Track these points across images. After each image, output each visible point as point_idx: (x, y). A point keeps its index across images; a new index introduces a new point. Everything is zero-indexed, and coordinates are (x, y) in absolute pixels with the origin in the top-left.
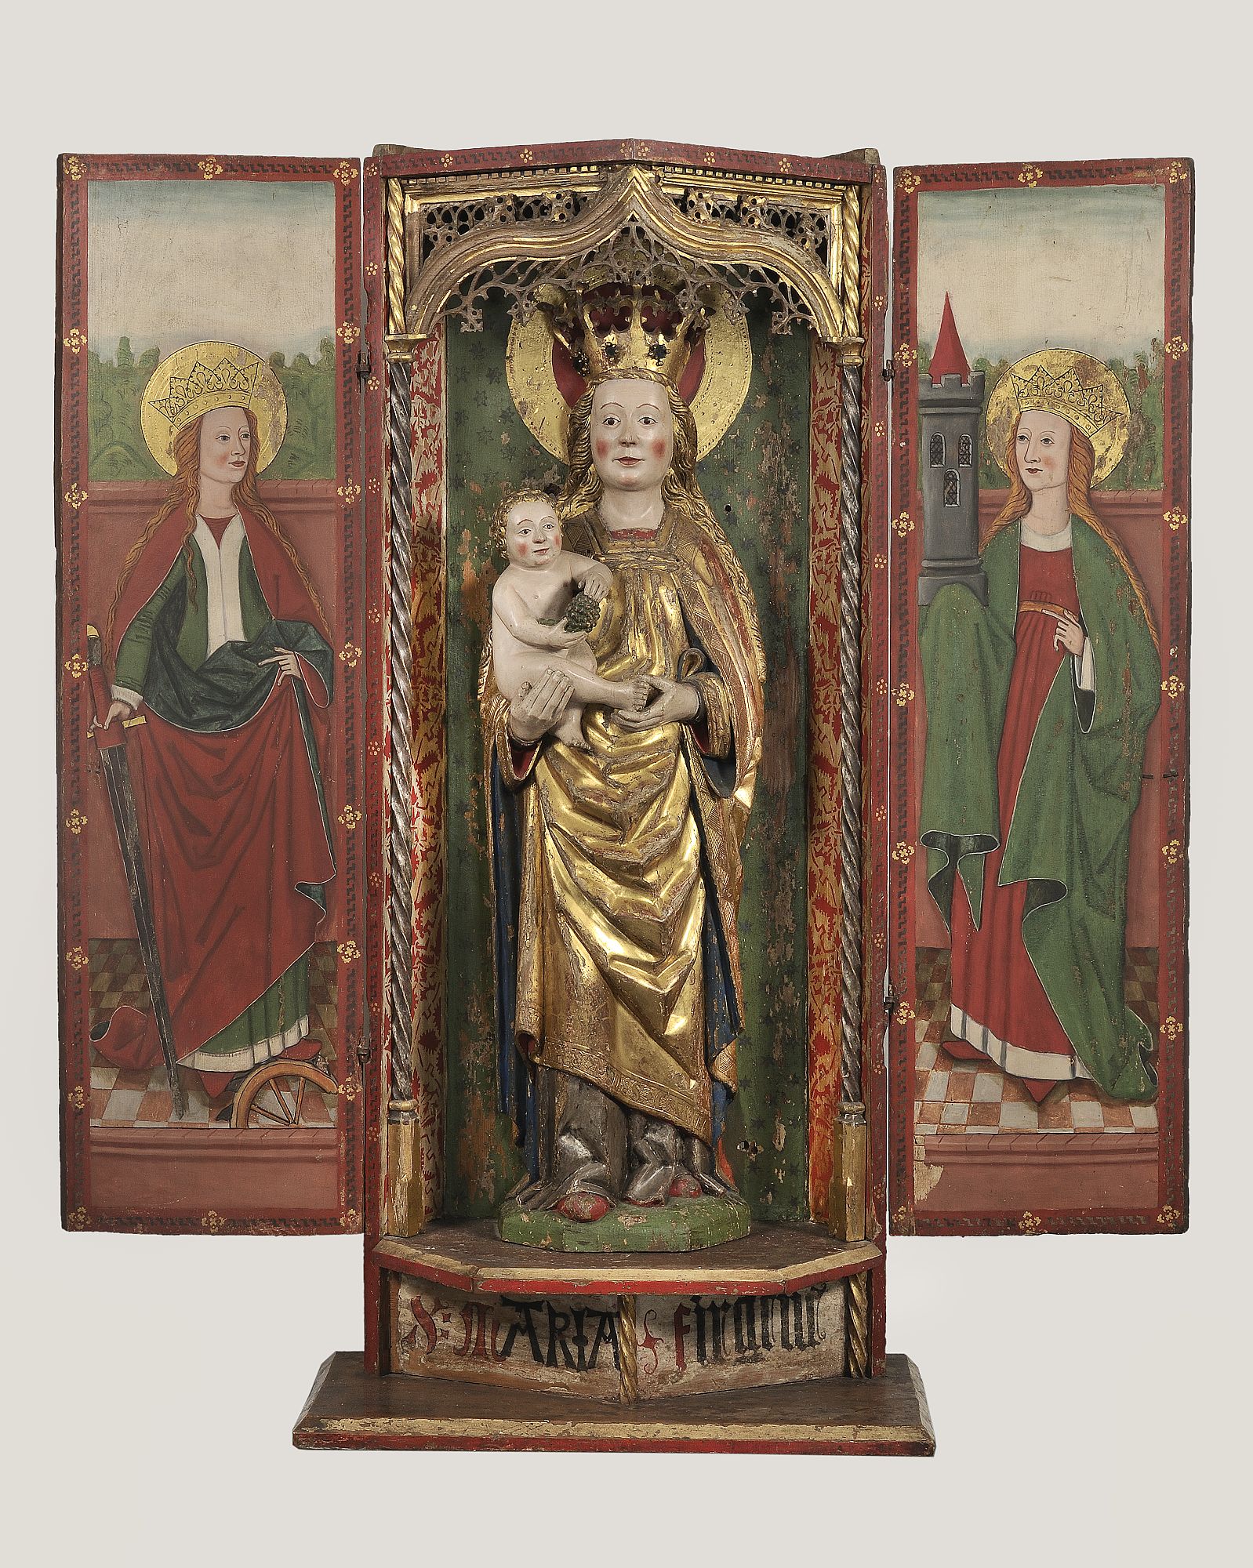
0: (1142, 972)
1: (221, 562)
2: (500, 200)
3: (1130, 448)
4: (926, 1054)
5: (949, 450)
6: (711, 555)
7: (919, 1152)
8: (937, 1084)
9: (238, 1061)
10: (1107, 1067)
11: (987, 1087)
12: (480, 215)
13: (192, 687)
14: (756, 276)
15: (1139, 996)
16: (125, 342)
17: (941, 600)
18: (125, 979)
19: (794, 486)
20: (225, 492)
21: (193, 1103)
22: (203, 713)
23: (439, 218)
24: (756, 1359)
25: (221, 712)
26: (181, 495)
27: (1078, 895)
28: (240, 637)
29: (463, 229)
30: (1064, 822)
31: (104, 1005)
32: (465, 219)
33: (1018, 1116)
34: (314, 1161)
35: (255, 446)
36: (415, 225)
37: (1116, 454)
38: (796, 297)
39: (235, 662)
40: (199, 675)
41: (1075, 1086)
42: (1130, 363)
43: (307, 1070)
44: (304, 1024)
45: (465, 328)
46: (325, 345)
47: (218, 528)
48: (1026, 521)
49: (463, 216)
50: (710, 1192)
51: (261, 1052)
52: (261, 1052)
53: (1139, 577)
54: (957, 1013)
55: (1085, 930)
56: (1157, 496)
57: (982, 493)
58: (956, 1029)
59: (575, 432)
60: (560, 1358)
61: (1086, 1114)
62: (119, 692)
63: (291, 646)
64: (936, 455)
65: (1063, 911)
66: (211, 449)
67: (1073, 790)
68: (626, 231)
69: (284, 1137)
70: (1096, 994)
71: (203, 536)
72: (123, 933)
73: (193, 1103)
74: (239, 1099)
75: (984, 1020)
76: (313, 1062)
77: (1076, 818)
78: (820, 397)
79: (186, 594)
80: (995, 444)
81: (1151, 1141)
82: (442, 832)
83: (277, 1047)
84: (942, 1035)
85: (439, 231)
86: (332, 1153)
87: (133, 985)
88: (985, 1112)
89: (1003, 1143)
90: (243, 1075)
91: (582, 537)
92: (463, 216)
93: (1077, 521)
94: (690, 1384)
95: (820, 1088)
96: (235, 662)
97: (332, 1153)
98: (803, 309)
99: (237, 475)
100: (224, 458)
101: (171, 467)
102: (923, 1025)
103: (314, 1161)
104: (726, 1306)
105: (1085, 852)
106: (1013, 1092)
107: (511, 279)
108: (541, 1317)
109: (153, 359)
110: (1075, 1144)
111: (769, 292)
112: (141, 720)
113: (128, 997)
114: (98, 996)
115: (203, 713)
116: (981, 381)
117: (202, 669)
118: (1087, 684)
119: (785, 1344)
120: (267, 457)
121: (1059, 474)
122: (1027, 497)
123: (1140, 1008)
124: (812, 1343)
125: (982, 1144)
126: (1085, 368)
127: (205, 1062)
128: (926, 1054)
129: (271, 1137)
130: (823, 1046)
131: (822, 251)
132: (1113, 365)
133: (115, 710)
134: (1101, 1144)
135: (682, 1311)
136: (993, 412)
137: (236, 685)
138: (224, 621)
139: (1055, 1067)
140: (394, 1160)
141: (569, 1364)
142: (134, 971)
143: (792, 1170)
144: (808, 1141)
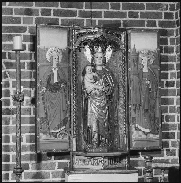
2: (86, 32)
3: (154, 61)
4: (134, 129)
7: (133, 140)
9: (57, 131)
10: (153, 131)
11: (140, 133)
12: (84, 34)
13: (52, 87)
15: (157, 122)
16: (44, 47)
17: (134, 78)
19: (116, 66)
20: (56, 64)
21: (52, 136)
23: (79, 34)
24: (116, 164)
25: (55, 90)
26: (51, 65)
28: (57, 81)
29: (82, 36)
30: (148, 103)
31: (42, 125)
32: (82, 35)
33: (144, 136)
34: (65, 143)
36: (76, 35)
37: (152, 62)
40: (53, 86)
41: (150, 132)
43: (65, 132)
44: (64, 126)
47: (55, 69)
48: (143, 69)
49: (82, 34)
51: (60, 130)
52: (60, 130)
53: (155, 75)
54: (137, 124)
55: (151, 115)
56: (157, 66)
57: (138, 66)
58: (137, 126)
61: (151, 136)
62: (44, 88)
63: (63, 83)
64: (133, 62)
67: (149, 99)
69: (62, 140)
70: (152, 121)
71: (53, 70)
72: (44, 116)
73: (52, 136)
74: (57, 136)
76: (65, 131)
77: (149, 102)
78: (119, 56)
79: (51, 77)
81: (158, 139)
86: (67, 142)
87: (45, 123)
88: (140, 136)
89: (142, 139)
90: (57, 133)
91: (94, 70)
95: (121, 134)
96: (57, 84)
97: (67, 142)
99: (57, 63)
100: (55, 61)
101: (50, 62)
103: (65, 143)
105: (150, 106)
106: (143, 133)
107: (88, 41)
109: (48, 49)
110: (150, 139)
112: (46, 91)
113: (45, 124)
114: (41, 124)
117: (53, 85)
120: (60, 61)
121: (147, 64)
123: (157, 123)
124: (122, 163)
125: (140, 139)
126: (149, 52)
127: (53, 131)
128: (134, 129)
129: (61, 140)
130: (121, 129)
132: (152, 52)
133: (43, 90)
134: (153, 139)
137: (57, 87)
138: (56, 80)
142: (45, 121)
143: (118, 144)
144: (119, 140)
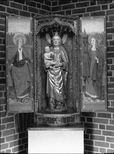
0: (103, 88)
1: (20, 53)
5: (85, 42)
6: (64, 52)
8: (85, 98)
9: (23, 97)
11: (89, 98)
12: (43, 22)
14: (67, 27)
16: (12, 33)
18: (12, 90)
22: (19, 66)
27: (97, 81)
35: (23, 43)
38: (71, 29)
39: (22, 61)
40: (18, 63)
41: (97, 98)
42: (101, 34)
44: (28, 94)
45: (42, 32)
46: (29, 33)
49: (42, 22)
50: (64, 108)
51: (25, 96)
52: (25, 96)
54: (86, 92)
58: (86, 93)
59: (52, 41)
60: (51, 123)
61: (98, 101)
62: (11, 64)
63: (27, 60)
65: (96, 83)
66: (19, 42)
68: (56, 22)
71: (19, 50)
73: (18, 101)
74: (23, 101)
75: (89, 93)
76: (29, 97)
77: (97, 74)
80: (89, 41)
82: (39, 53)
83: (26, 96)
84: (85, 94)
85: (39, 23)
87: (13, 91)
88: (89, 101)
89: (90, 104)
92: (42, 22)
93: (97, 48)
94: (49, 75)
96: (22, 61)
98: (72, 30)
99: (22, 45)
102: (83, 93)
104: (66, 118)
108: (50, 119)
110: (97, 104)
111: (69, 28)
115: (19, 66)
116: (88, 36)
118: (98, 62)
119: (71, 121)
120: (24, 43)
121: (95, 44)
122: (92, 46)
123: (103, 91)
127: (20, 97)
128: (84, 95)
131: (73, 25)
132: (100, 34)
133: (11, 66)
135: (62, 118)
136: (89, 39)
137: (22, 63)
138: (21, 58)
139: (95, 97)
140: (36, 106)
141: (52, 123)
